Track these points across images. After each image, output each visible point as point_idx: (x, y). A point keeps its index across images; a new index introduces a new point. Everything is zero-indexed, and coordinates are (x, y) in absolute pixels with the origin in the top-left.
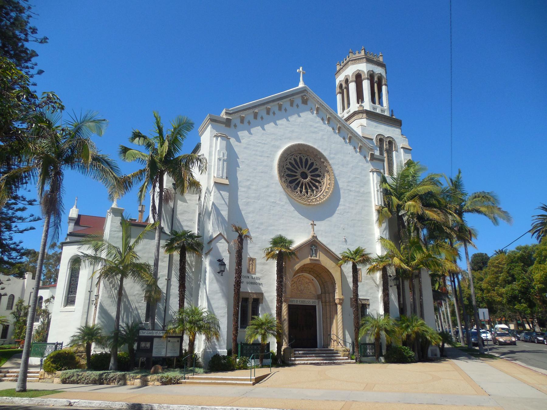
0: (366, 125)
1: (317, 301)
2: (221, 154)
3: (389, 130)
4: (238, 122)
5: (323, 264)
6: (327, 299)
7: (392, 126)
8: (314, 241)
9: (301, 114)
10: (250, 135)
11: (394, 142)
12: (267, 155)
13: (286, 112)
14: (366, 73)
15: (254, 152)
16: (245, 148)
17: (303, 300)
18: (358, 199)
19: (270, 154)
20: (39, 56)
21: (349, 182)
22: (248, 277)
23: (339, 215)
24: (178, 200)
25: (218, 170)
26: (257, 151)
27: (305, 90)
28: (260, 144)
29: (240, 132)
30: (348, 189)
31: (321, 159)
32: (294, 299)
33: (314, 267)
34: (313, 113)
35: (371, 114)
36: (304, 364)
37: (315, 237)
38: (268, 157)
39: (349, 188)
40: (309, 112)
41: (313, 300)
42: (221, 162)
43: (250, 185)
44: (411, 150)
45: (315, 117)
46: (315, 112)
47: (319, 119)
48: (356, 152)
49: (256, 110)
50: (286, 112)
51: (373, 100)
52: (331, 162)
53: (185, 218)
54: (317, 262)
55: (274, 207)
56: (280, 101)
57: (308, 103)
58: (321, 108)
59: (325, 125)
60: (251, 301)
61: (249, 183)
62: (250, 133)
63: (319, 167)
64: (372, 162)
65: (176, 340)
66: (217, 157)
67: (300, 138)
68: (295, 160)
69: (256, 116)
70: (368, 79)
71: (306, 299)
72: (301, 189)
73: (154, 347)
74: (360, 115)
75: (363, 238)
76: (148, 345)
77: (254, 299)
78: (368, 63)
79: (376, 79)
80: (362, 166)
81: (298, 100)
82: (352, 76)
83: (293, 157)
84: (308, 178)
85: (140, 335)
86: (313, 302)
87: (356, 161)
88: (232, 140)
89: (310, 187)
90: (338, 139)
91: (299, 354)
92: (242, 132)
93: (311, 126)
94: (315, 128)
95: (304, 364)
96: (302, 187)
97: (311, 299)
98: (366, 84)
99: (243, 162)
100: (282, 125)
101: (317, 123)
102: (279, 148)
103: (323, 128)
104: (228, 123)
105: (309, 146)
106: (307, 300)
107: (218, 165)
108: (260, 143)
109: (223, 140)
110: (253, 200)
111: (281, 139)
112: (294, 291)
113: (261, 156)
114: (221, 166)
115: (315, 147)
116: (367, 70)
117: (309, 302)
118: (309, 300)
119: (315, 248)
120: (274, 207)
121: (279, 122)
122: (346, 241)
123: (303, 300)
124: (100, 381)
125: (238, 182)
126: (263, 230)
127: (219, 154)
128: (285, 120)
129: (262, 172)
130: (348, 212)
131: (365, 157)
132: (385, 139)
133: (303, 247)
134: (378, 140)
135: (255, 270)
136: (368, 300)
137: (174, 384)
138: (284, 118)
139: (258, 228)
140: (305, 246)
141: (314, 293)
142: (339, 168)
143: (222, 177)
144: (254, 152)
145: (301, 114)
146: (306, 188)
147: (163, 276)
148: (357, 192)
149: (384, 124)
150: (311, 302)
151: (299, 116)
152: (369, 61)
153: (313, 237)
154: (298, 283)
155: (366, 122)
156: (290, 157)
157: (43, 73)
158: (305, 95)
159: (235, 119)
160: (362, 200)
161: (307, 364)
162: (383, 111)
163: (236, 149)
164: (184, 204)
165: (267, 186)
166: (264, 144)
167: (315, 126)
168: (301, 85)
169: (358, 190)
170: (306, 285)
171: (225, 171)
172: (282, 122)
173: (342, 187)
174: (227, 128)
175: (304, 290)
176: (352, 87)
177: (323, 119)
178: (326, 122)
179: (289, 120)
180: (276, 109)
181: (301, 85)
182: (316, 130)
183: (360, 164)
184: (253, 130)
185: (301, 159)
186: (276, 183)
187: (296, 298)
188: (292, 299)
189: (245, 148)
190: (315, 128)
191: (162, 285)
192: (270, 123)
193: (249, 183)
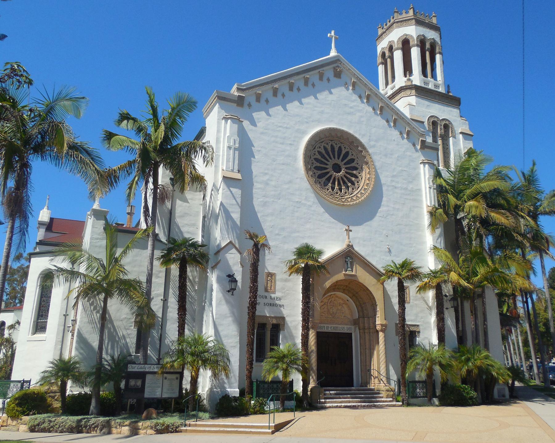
0: (415, 105)
1: (353, 327)
2: (232, 141)
3: (444, 111)
4: (253, 100)
6: (366, 325)
7: (448, 106)
9: (332, 90)
10: (268, 117)
12: (290, 142)
14: (415, 38)
16: (262, 133)
17: (335, 326)
18: (405, 198)
19: (294, 141)
21: (393, 176)
22: (266, 297)
25: (228, 161)
27: (339, 60)
28: (280, 129)
29: (256, 113)
30: (393, 186)
31: (358, 147)
32: (324, 325)
33: (349, 284)
34: (347, 89)
36: (337, 407)
37: (350, 246)
38: (291, 144)
39: (394, 184)
40: (343, 88)
41: (348, 326)
42: (231, 152)
43: (268, 180)
46: (351, 88)
47: (355, 97)
48: (403, 138)
49: (276, 86)
53: (186, 222)
54: (353, 278)
57: (342, 76)
58: (358, 82)
60: (269, 327)
62: (268, 115)
63: (355, 158)
67: (332, 121)
69: (275, 92)
70: (417, 45)
71: (339, 324)
72: (333, 186)
74: (408, 92)
76: (139, 383)
77: (273, 325)
79: (428, 46)
80: (410, 156)
81: (329, 72)
82: (417, 38)
83: (323, 144)
84: (342, 171)
85: (129, 370)
86: (349, 329)
87: (403, 150)
89: (344, 183)
90: (380, 121)
91: (331, 394)
94: (351, 108)
95: (337, 407)
96: (334, 183)
97: (346, 325)
99: (259, 151)
100: (308, 104)
102: (304, 133)
103: (361, 108)
106: (340, 326)
107: (228, 155)
108: (280, 127)
111: (307, 122)
112: (324, 315)
113: (282, 144)
115: (351, 131)
116: (416, 34)
117: (344, 328)
119: (351, 261)
121: (304, 100)
122: (390, 251)
123: (335, 326)
125: (253, 177)
126: (285, 237)
128: (312, 97)
129: (283, 164)
132: (439, 122)
134: (431, 123)
135: (275, 288)
136: (418, 326)
137: (172, 432)
138: (311, 95)
139: (278, 234)
140: (338, 258)
141: (349, 317)
145: (332, 90)
146: (339, 184)
148: (404, 189)
151: (331, 93)
152: (419, 23)
153: (349, 246)
154: (329, 305)
156: (319, 145)
158: (338, 67)
159: (250, 97)
160: (410, 199)
161: (340, 407)
162: (436, 86)
163: (251, 135)
164: (185, 204)
165: (290, 182)
166: (287, 128)
167: (351, 105)
168: (333, 53)
170: (340, 308)
172: (309, 100)
174: (239, 109)
175: (336, 313)
176: (398, 55)
177: (360, 97)
178: (365, 101)
180: (301, 84)
181: (333, 53)
182: (352, 110)
183: (408, 153)
184: (272, 111)
185: (333, 148)
187: (326, 324)
188: (322, 325)
189: (262, 133)
190: (351, 108)
191: (157, 307)
193: (266, 178)
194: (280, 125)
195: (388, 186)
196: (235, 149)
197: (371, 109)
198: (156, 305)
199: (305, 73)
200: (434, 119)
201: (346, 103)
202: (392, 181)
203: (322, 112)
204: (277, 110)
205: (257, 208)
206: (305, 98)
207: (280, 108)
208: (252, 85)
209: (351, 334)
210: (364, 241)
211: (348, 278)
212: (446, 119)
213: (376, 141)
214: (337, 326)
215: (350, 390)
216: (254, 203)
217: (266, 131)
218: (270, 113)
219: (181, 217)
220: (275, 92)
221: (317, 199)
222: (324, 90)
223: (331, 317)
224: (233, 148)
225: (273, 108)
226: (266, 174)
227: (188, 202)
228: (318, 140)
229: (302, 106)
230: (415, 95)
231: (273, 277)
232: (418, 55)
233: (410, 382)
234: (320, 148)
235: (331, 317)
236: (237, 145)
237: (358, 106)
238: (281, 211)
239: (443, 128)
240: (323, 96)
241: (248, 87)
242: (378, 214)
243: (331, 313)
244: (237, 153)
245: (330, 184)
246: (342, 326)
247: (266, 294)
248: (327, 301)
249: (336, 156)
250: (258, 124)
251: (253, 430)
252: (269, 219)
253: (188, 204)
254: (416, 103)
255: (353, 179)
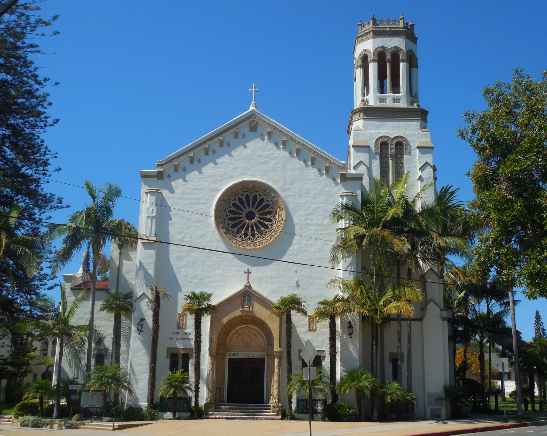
0: (362, 128)
2: (150, 211)
3: (399, 127)
4: (171, 171)
5: (257, 315)
7: (405, 120)
8: (247, 291)
9: (247, 144)
10: (185, 183)
11: (404, 142)
12: (203, 202)
13: (244, 138)
14: (372, 53)
15: (189, 201)
16: (179, 198)
17: (248, 353)
18: (320, 234)
19: (208, 200)
20: (53, 105)
21: (308, 214)
22: (178, 333)
23: (291, 256)
24: (124, 260)
25: (147, 228)
26: (192, 199)
27: (253, 115)
28: (195, 191)
29: (174, 182)
30: (306, 224)
31: (270, 192)
34: (263, 139)
35: (403, 111)
36: (219, 418)
37: (248, 287)
38: (204, 203)
39: (307, 222)
40: (259, 140)
41: (261, 353)
42: (150, 220)
43: (183, 237)
44: (433, 148)
45: (266, 144)
46: (266, 138)
47: (271, 146)
48: (321, 174)
49: (191, 154)
50: (244, 138)
51: (382, 89)
52: (282, 195)
53: (130, 277)
54: (250, 314)
55: (209, 257)
56: (219, 137)
57: (258, 129)
58: (273, 131)
59: (279, 150)
61: (182, 235)
62: (185, 180)
64: (344, 183)
65: (100, 393)
66: (146, 215)
67: (245, 174)
68: (240, 199)
69: (221, 144)
71: (253, 352)
72: (247, 232)
73: (82, 399)
75: (322, 279)
76: (77, 397)
78: (376, 38)
79: (388, 57)
80: (329, 191)
81: (245, 128)
82: (374, 53)
83: (237, 197)
84: (256, 218)
85: (70, 389)
87: (321, 187)
88: (165, 193)
89: (258, 228)
90: (297, 163)
91: (226, 408)
92: (176, 181)
93: (260, 156)
94: (266, 157)
95: (219, 418)
96: (247, 229)
97: (259, 352)
98: (373, 68)
99: (176, 214)
100: (222, 163)
101: (268, 150)
102: (218, 190)
103: (276, 155)
104: (160, 175)
105: (255, 181)
106: (253, 353)
107: (147, 223)
108: (196, 189)
109: (152, 196)
110: (186, 253)
111: (221, 180)
112: (238, 344)
113: (197, 204)
114: (149, 224)
115: (264, 181)
116: (374, 47)
117: (257, 355)
118: (257, 353)
120: (209, 257)
121: (219, 161)
122: (298, 285)
123: (248, 353)
124: (36, 425)
125: (170, 237)
126: (196, 283)
127: (148, 212)
128: (227, 156)
129: (197, 222)
130: (304, 251)
131: (334, 179)
132: (389, 142)
133: (234, 298)
134: (379, 145)
135: (186, 325)
136: (323, 351)
137: (75, 428)
138: (226, 154)
139: (190, 282)
140: (236, 297)
142: (295, 199)
143: (150, 235)
144: (189, 201)
145: (247, 144)
146: (252, 230)
147: (109, 334)
148: (319, 225)
149: (392, 120)
150: (259, 355)
151: (245, 147)
152: (377, 34)
153: (246, 286)
154: (243, 335)
155: (362, 124)
156: (228, 205)
157: (59, 121)
158: (253, 121)
159: (169, 169)
160: (325, 234)
161: (222, 418)
163: (169, 202)
164: (130, 262)
165: (203, 236)
166: (201, 189)
167: (266, 155)
168: (252, 107)
169: (320, 222)
170: (254, 337)
171: (154, 228)
172: (224, 160)
173: (297, 222)
174: (160, 181)
175: (250, 342)
177: (276, 144)
178: (281, 147)
179: (233, 155)
181: (252, 107)
182: (266, 159)
183: (326, 189)
184: (188, 177)
185: (247, 197)
186: (213, 231)
188: (236, 353)
189: (179, 198)
190: (266, 157)
191: (109, 343)
192: (209, 164)
193: (182, 235)
194: (195, 188)
195: (301, 225)
196: (153, 217)
197: (287, 154)
198: (108, 341)
199: (218, 136)
200: (384, 140)
201: (260, 154)
202: (306, 219)
203: (236, 168)
204: (193, 176)
205: (172, 262)
206: (219, 158)
207: (196, 172)
208: (169, 160)
209: (264, 359)
210: (272, 279)
211: (244, 314)
212: (399, 136)
213: (291, 184)
214: (250, 353)
215: (248, 406)
216: (170, 258)
217: (182, 196)
218: (187, 179)
219: (128, 273)
220: (221, 144)
221: (227, 247)
222: (238, 146)
223: (244, 345)
224: (150, 218)
225: (190, 174)
226: (181, 232)
227: (132, 261)
228: (251, 187)
229: (217, 166)
230: (363, 118)
231: (184, 317)
232: (373, 71)
233: (300, 400)
234: (235, 200)
235: (244, 345)
236: (154, 214)
237: (274, 154)
238: (193, 262)
239: (394, 147)
240: (238, 152)
241: (166, 161)
242: (288, 253)
243: (245, 342)
244: (154, 220)
245: (243, 232)
246: (255, 353)
247: (180, 331)
248: (242, 333)
249: (243, 208)
250: (176, 192)
251: (106, 428)
252: (183, 270)
253: (132, 262)
254: (363, 127)
255: (267, 223)
